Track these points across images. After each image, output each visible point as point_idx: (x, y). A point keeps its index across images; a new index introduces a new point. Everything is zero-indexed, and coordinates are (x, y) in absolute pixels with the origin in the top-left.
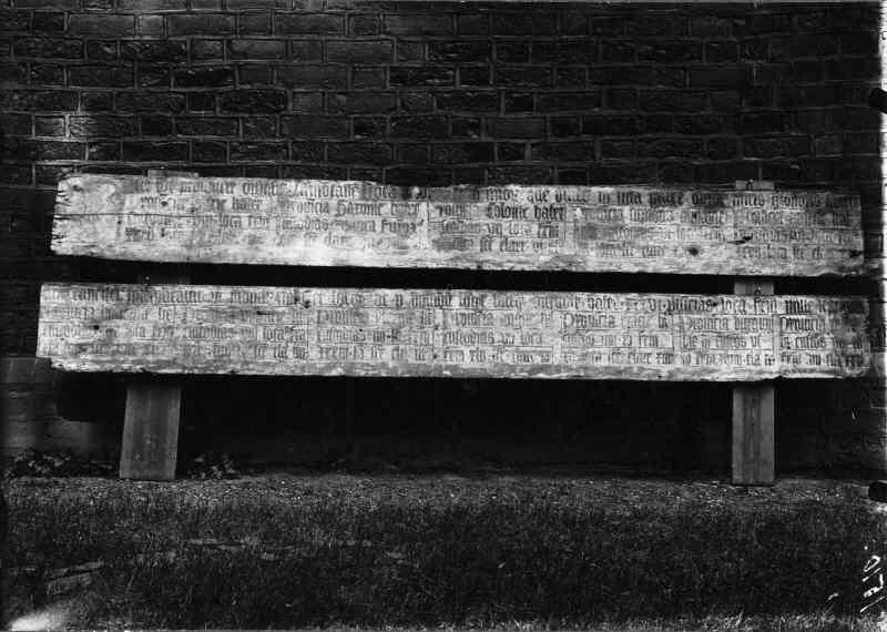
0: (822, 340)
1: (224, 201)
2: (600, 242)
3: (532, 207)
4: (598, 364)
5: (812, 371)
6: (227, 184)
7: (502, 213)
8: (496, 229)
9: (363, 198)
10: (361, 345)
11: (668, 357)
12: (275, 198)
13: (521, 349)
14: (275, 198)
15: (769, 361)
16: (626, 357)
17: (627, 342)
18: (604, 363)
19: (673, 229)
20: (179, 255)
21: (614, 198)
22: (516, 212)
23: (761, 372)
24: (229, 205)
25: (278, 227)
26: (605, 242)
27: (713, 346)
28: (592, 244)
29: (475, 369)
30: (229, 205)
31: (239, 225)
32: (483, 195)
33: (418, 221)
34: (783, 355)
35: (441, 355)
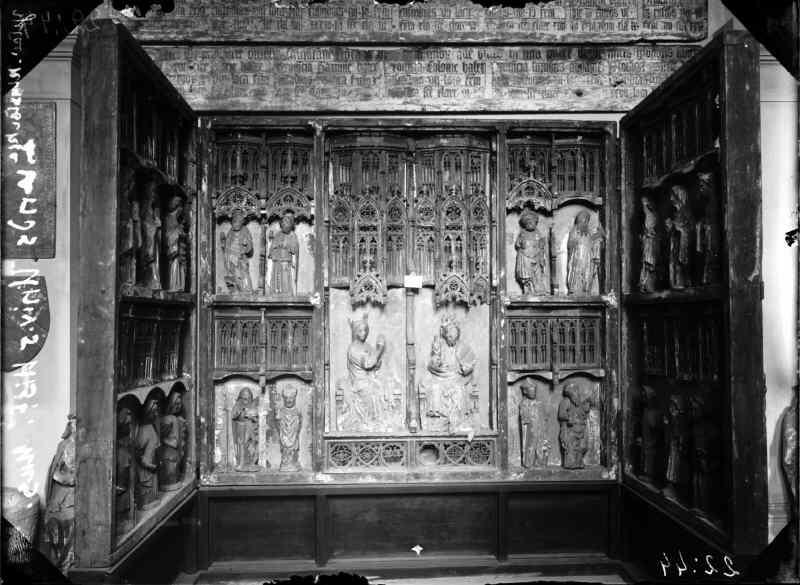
0: (673, 11)
1: (234, 64)
2: (511, 88)
3: (460, 63)
4: (511, 31)
5: (665, 34)
6: (236, 52)
7: (439, 68)
8: (435, 81)
9: (337, 60)
10: (340, 19)
11: (562, 26)
12: (272, 62)
13: (457, 20)
14: (272, 62)
15: (634, 27)
16: (531, 27)
17: (532, 14)
18: (515, 30)
19: (564, 77)
20: (207, 106)
21: (521, 55)
22: (448, 67)
23: (628, 36)
24: (238, 67)
25: (275, 83)
26: (515, 88)
27: (594, 15)
28: (505, 90)
29: (423, 36)
30: (238, 67)
31: (246, 82)
32: (424, 55)
33: (378, 75)
34: (644, 23)
35: (397, 27)
